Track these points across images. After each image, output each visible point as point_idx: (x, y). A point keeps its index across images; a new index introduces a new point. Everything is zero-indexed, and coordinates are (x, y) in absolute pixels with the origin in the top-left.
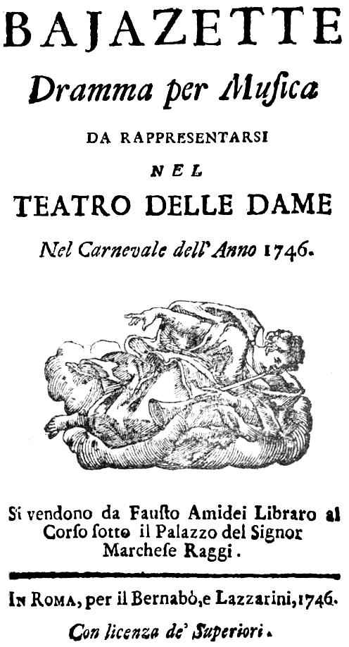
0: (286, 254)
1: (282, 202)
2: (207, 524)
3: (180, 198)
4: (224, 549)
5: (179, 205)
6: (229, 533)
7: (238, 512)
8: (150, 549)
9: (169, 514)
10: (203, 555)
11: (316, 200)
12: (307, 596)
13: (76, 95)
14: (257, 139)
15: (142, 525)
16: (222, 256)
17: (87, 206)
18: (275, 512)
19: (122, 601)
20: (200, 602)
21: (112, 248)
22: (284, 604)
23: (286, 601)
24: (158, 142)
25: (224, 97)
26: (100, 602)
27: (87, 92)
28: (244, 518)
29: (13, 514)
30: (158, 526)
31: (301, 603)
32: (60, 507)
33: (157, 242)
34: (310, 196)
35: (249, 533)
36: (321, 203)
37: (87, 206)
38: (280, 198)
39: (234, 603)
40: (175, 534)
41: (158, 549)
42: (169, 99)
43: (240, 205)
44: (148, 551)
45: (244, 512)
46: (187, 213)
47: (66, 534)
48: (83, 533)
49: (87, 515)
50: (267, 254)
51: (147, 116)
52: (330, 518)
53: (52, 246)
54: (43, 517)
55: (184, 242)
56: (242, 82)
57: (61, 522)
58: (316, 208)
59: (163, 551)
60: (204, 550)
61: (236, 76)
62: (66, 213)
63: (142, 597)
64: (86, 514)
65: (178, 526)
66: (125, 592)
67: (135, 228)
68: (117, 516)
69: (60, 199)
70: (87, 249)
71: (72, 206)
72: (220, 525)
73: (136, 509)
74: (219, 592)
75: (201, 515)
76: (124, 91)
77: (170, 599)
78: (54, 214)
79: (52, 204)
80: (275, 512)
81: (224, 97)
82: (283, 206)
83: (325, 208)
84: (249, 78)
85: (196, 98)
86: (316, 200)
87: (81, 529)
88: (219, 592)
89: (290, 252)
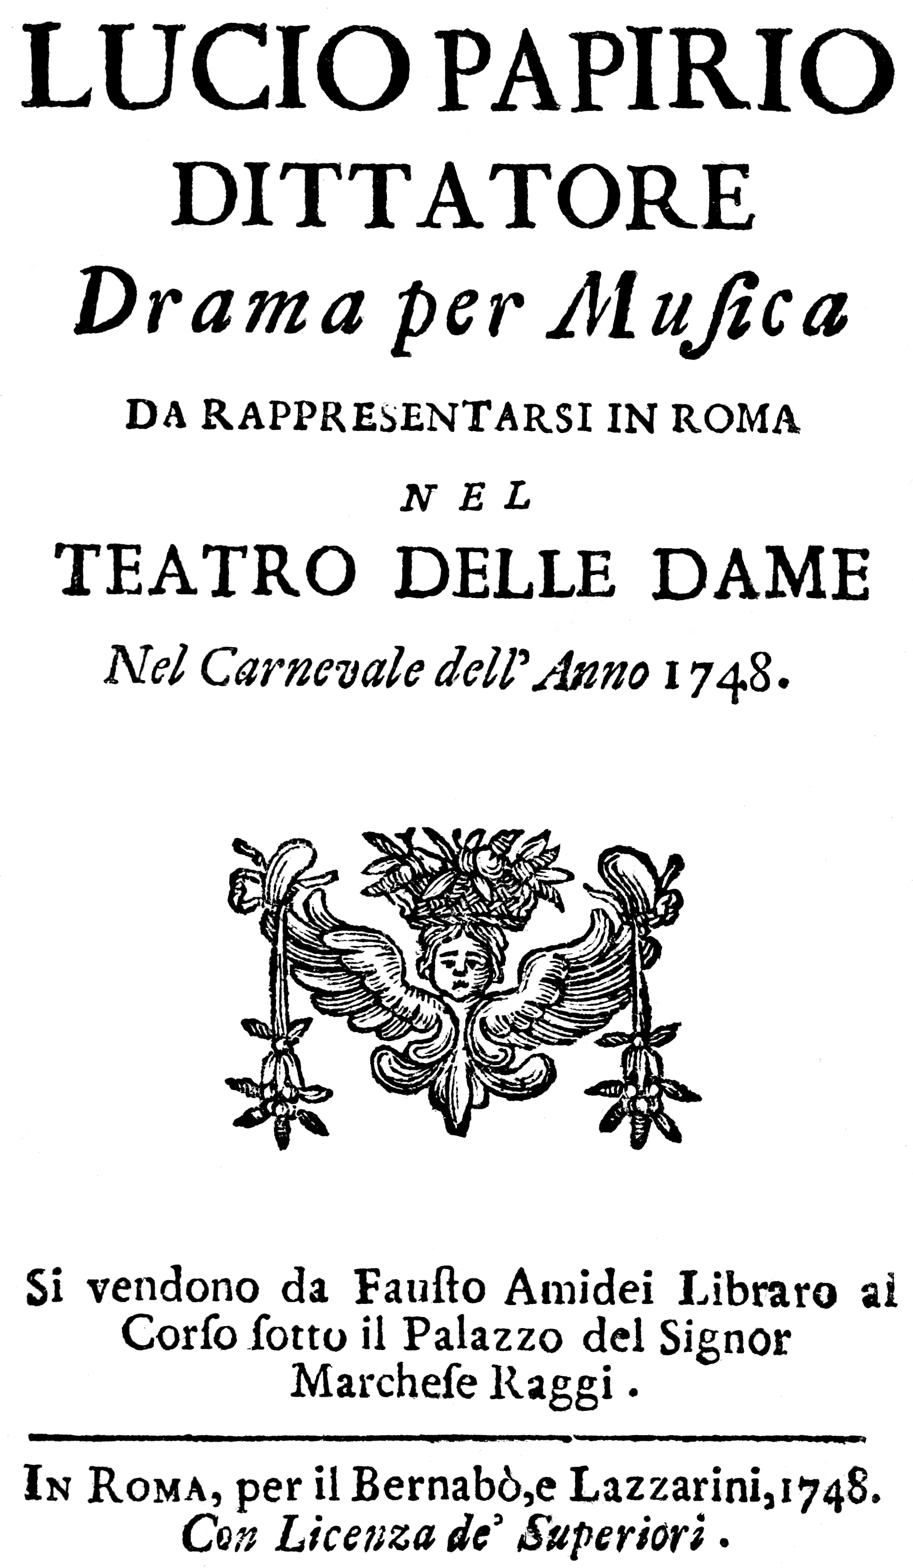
0: (721, 685)
1: (742, 568)
2: (541, 1317)
3: (485, 552)
4: (592, 1380)
5: (482, 572)
6: (601, 1338)
7: (629, 1287)
8: (412, 1378)
9: (458, 1290)
10: (537, 1393)
11: (829, 564)
12: (803, 1483)
13: (208, 315)
14: (563, 425)
15: (367, 1319)
16: (562, 686)
17: (244, 572)
18: (731, 1286)
19: (373, 1341)
20: (528, 1495)
21: (287, 663)
22: (743, 1499)
23: (749, 1493)
24: (300, 426)
25: (560, 332)
26: (272, 1493)
27: (240, 311)
28: (648, 1300)
29: (41, 1292)
30: (410, 1320)
31: (786, 1499)
32: (177, 1269)
33: (401, 649)
34: (814, 553)
35: (653, 1338)
36: (844, 572)
37: (244, 572)
38: (737, 556)
39: (618, 1499)
40: (454, 1340)
41: (432, 1380)
42: (405, 331)
43: (635, 573)
44: (407, 1383)
45: (647, 1286)
46: (504, 592)
47: (182, 1339)
48: (226, 1338)
49: (247, 1290)
50: (672, 684)
51: (354, 368)
52: (870, 1302)
53: (136, 657)
54: (132, 1293)
55: (462, 649)
56: (608, 289)
57: (177, 1308)
58: (830, 584)
59: (443, 1382)
60: (349, 1378)
61: (594, 279)
62: (186, 589)
63: (380, 1483)
64: (246, 1290)
65: (461, 1318)
66: (334, 1470)
67: (369, 622)
68: (320, 1296)
69: (173, 554)
70: (221, 666)
71: (204, 572)
72: (576, 1320)
73: (371, 1278)
74: (579, 1471)
75: (537, 1294)
76: (280, 309)
77: (452, 1488)
78: (158, 590)
79: (152, 565)
80: (731, 1287)
81: (560, 332)
82: (744, 577)
83: (855, 585)
84: (627, 281)
85: (494, 330)
86: (829, 564)
87: (273, 1329)
88: (579, 1471)
89: (729, 680)
